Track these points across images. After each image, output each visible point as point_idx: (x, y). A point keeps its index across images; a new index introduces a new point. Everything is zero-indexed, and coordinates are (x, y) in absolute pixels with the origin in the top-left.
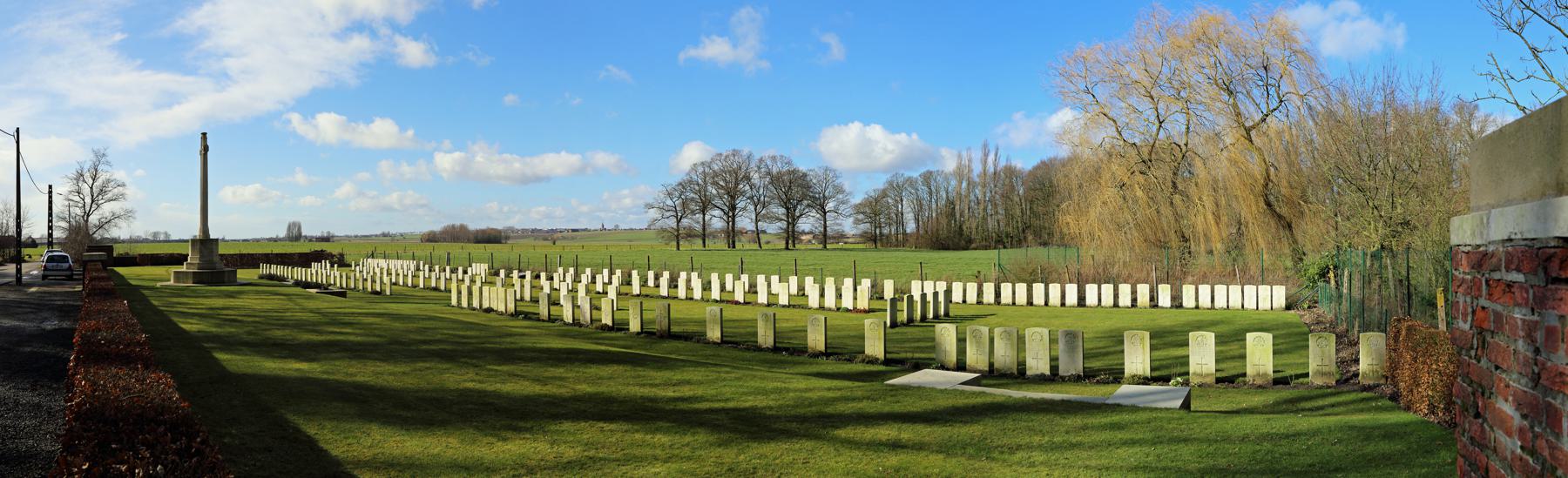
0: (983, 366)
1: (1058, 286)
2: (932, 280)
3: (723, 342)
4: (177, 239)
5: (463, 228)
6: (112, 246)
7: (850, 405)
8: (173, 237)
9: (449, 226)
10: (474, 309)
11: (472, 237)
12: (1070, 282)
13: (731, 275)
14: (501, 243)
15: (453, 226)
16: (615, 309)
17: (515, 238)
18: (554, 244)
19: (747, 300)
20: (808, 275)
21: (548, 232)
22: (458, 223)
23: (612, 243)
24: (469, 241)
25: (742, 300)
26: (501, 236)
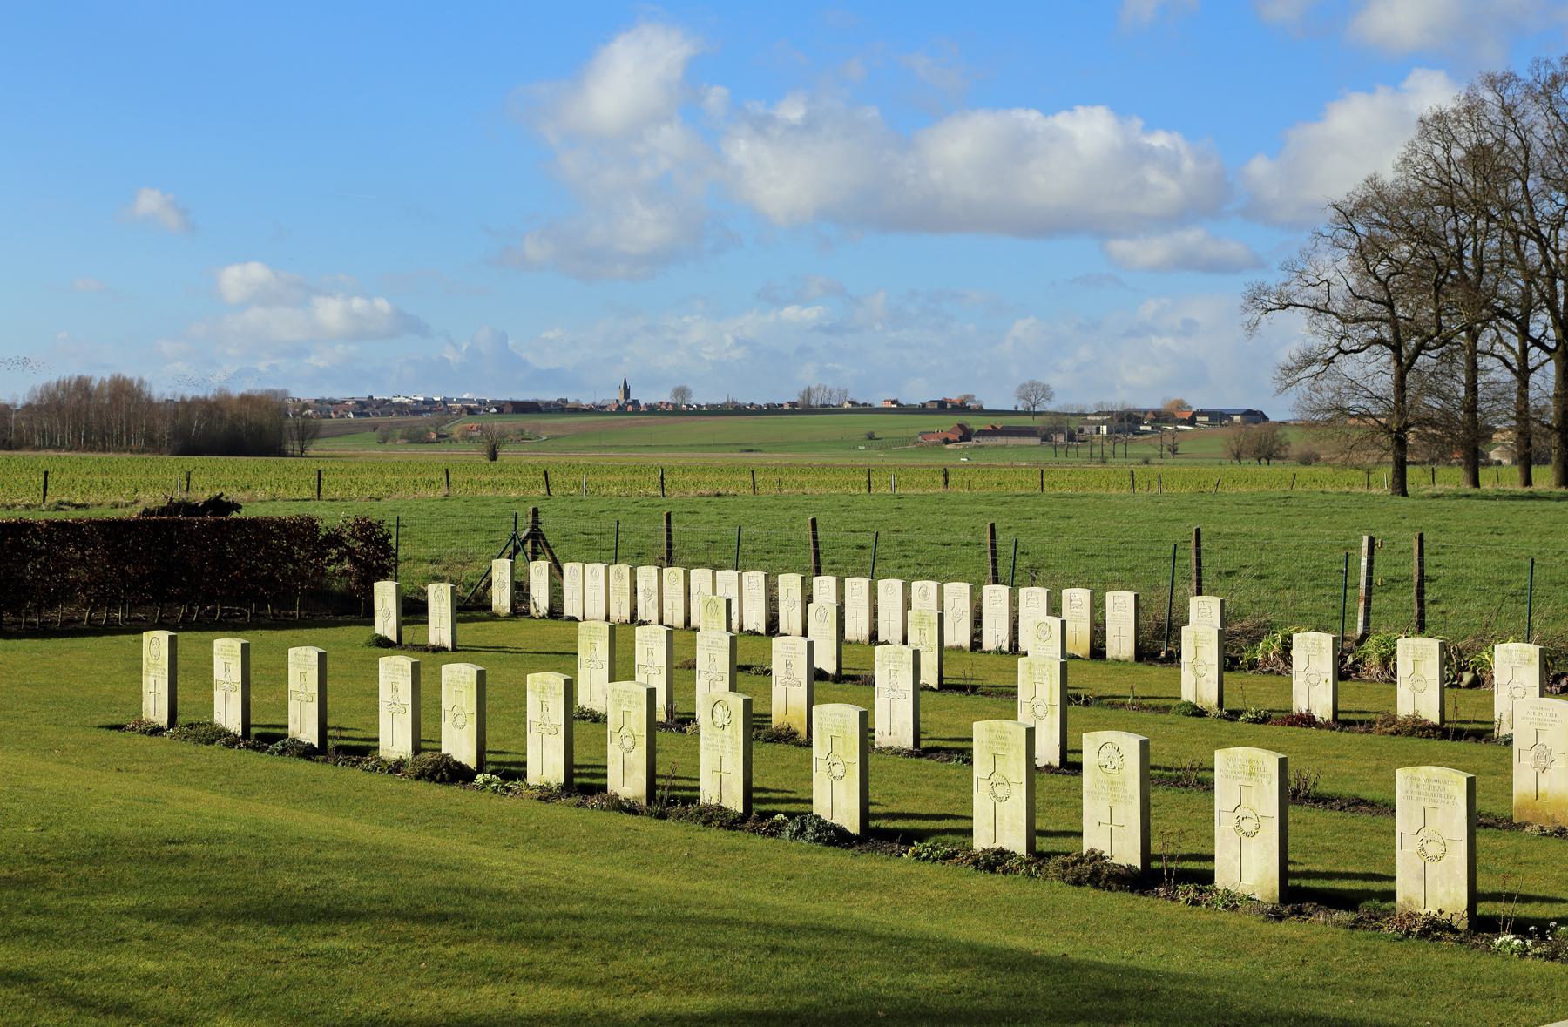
0: (1267, 893)
1: (864, 583)
2: (831, 572)
3: (1483, 925)
4: (719, 399)
5: (124, 393)
6: (1559, 485)
7: (132, 903)
8: (700, 398)
9: (63, 386)
10: (456, 774)
11: (164, 428)
12: (996, 582)
13: (1129, 597)
14: (282, 453)
15: (82, 385)
16: (661, 716)
17: (339, 432)
18: (493, 457)
19: (1232, 703)
20: (787, 570)
21: (416, 409)
22: (100, 375)
23: (684, 458)
24: (152, 445)
25: (1323, 711)
26: (281, 429)
